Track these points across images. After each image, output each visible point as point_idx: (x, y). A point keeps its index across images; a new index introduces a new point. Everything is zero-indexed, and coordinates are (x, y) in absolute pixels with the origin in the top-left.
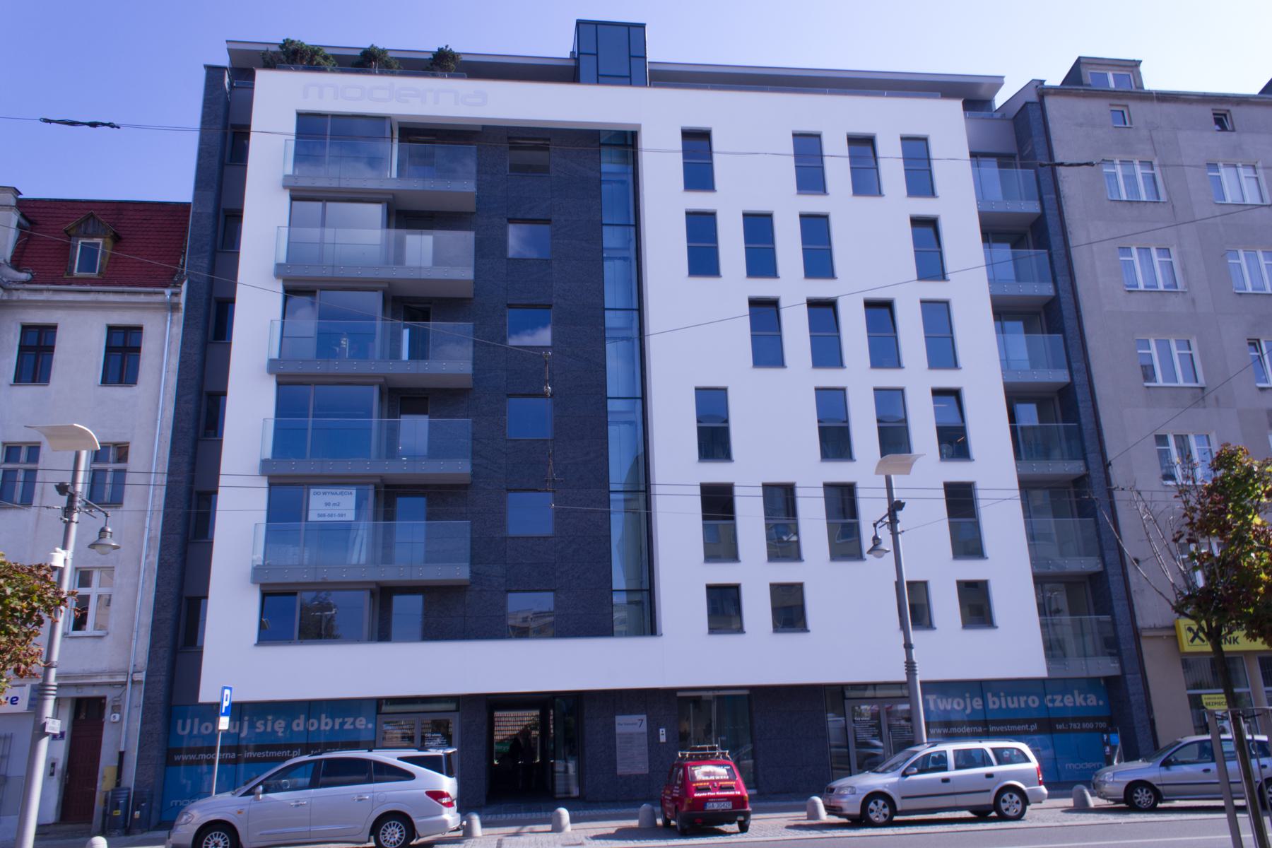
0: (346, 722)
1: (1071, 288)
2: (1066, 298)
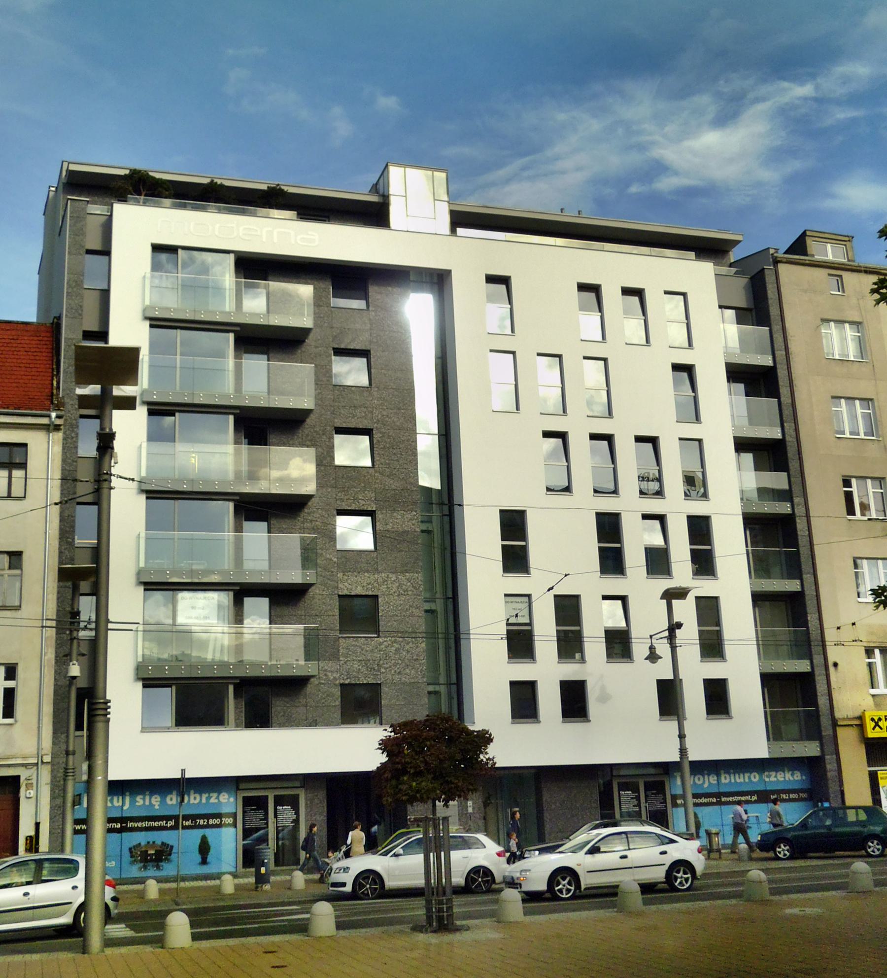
0: (212, 797)
1: (795, 433)
2: (809, 592)
